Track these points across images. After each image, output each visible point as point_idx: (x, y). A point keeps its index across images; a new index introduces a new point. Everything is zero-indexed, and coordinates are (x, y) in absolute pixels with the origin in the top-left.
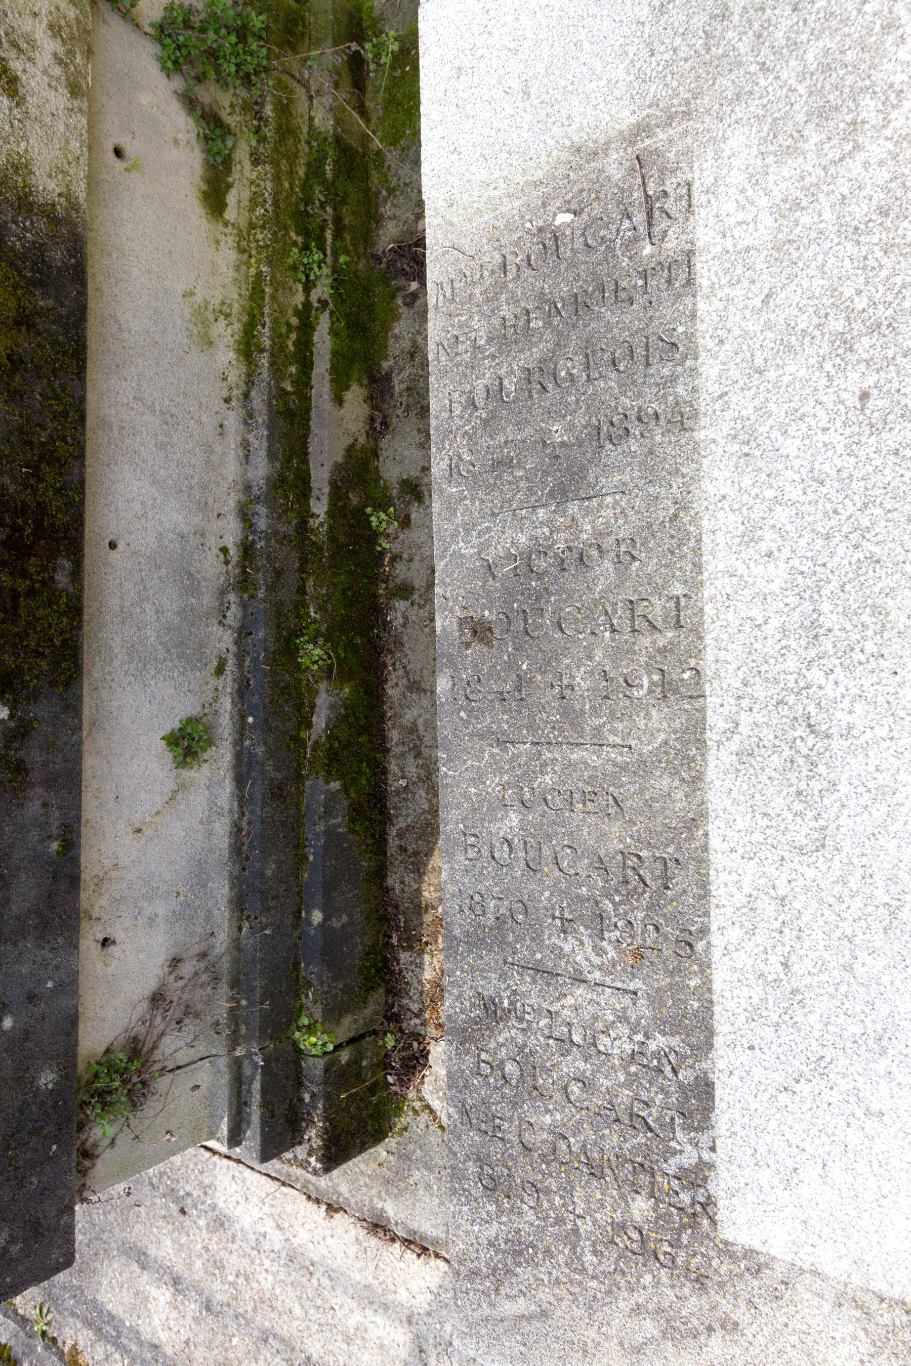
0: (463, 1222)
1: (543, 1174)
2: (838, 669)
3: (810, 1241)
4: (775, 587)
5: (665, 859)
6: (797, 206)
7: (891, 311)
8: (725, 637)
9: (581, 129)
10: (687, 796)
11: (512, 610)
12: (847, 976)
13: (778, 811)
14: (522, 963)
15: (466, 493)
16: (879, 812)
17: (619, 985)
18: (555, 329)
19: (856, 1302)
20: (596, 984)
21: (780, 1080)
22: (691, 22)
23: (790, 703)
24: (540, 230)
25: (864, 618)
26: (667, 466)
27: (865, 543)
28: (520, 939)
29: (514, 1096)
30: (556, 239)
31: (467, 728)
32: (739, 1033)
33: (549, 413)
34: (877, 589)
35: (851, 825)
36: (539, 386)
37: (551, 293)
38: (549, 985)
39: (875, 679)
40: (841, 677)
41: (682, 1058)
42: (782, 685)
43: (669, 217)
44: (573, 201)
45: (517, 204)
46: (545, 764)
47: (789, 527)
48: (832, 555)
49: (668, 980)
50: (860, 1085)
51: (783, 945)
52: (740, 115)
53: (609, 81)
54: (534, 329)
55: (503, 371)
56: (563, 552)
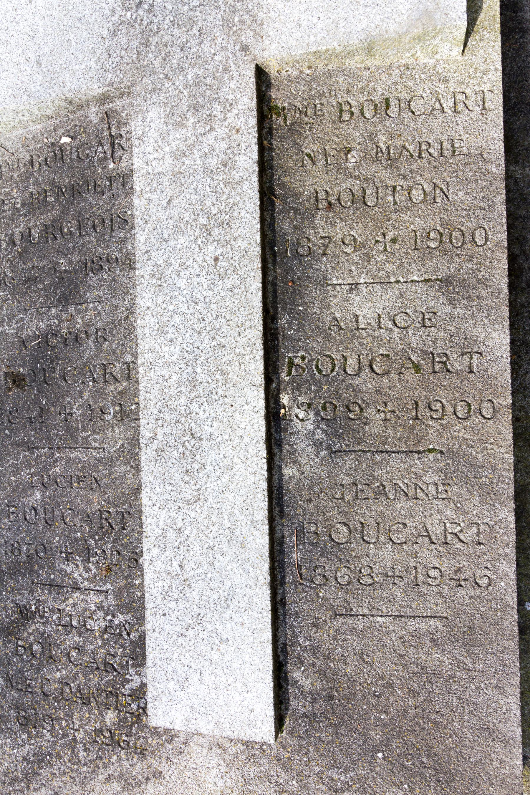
0: (8, 749)
1: (55, 709)
2: (205, 404)
3: (194, 717)
4: (174, 358)
5: (122, 512)
6: (183, 154)
7: (228, 216)
8: (149, 385)
9: (71, 91)
10: (134, 476)
11: (37, 368)
12: (211, 568)
13: (177, 481)
14: (43, 582)
15: (9, 296)
16: (225, 479)
17: (98, 588)
18: (61, 203)
19: (218, 745)
20: (86, 589)
21: (179, 630)
22: (130, 44)
23: (183, 422)
24: (53, 144)
25: (217, 376)
26: (122, 289)
27: (217, 337)
28: (42, 567)
29: (38, 665)
30: (62, 151)
31: (9, 440)
32: (158, 607)
33: (58, 252)
34: (223, 361)
35: (212, 486)
36: (52, 236)
37: (59, 182)
38: (58, 593)
39: (223, 409)
40: (207, 408)
41: (132, 625)
42: (178, 412)
43: (123, 149)
44: (72, 131)
45: (39, 127)
46: (56, 461)
47: (181, 326)
48: (202, 342)
49: (125, 582)
50: (217, 627)
51: (180, 555)
52: (155, 100)
53: (86, 66)
54: (49, 202)
55: (31, 225)
56: (66, 335)
